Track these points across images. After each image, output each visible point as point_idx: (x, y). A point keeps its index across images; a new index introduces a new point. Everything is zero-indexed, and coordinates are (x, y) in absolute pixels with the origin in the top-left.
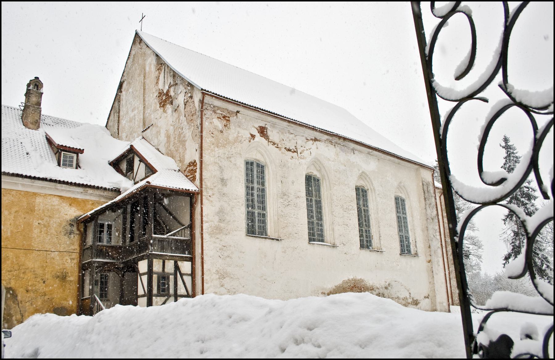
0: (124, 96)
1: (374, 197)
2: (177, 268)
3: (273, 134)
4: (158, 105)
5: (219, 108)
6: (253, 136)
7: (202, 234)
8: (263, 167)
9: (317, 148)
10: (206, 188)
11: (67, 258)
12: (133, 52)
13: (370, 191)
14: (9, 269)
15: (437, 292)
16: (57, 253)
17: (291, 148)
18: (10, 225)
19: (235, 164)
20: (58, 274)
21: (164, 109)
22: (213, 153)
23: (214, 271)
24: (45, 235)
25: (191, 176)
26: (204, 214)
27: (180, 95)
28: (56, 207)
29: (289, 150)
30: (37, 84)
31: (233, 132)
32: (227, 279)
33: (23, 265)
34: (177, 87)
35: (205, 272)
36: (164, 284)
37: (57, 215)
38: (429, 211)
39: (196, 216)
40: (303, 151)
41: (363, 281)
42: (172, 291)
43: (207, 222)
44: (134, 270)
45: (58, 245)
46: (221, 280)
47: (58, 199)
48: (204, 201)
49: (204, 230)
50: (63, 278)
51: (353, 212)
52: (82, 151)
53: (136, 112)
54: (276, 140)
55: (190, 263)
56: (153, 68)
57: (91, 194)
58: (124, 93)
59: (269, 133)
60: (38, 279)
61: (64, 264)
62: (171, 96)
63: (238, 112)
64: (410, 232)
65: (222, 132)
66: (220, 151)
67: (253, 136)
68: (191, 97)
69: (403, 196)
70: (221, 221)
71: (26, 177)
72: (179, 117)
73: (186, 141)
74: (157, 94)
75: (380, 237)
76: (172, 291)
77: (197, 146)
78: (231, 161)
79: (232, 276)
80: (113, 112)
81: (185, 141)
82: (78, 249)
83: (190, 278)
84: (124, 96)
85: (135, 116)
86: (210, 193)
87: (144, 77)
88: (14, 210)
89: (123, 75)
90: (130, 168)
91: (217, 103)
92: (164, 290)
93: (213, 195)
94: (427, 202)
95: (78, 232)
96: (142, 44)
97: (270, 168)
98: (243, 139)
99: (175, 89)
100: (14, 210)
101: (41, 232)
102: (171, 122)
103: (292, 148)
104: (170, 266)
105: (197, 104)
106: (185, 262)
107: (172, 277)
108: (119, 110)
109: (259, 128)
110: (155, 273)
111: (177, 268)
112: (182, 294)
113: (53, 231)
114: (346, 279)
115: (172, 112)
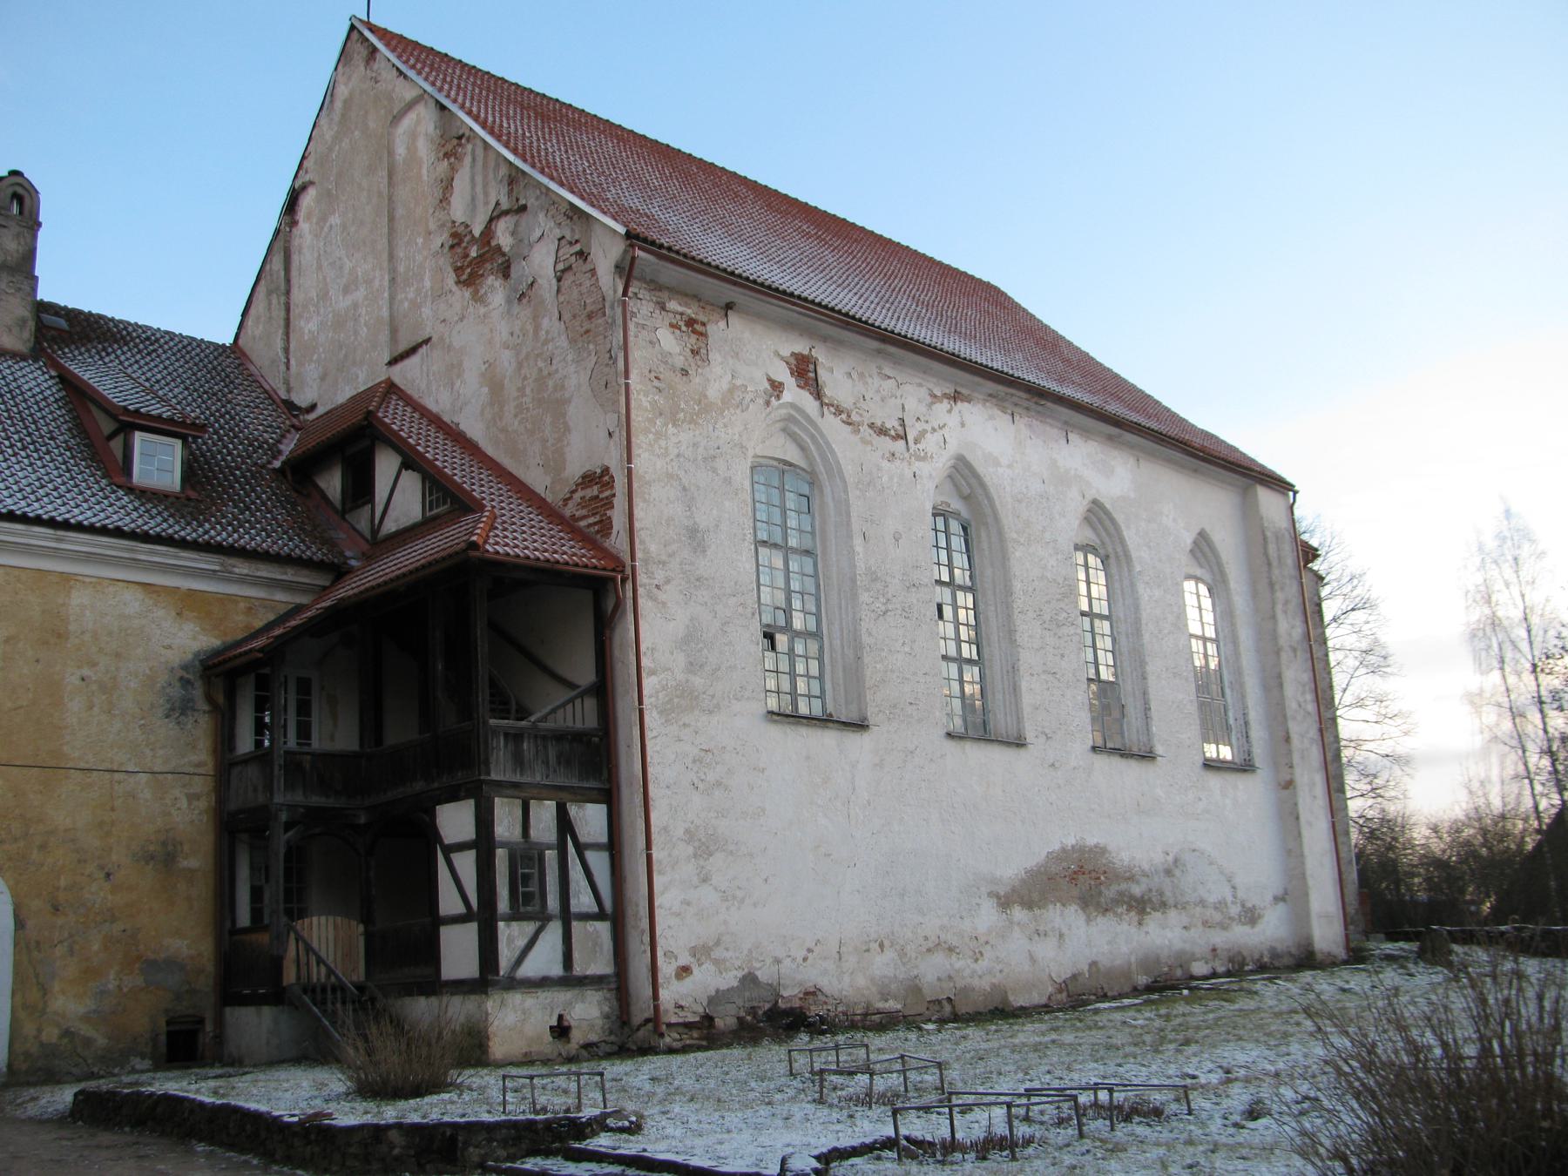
1: (1126, 582)
2: (565, 825)
4: (451, 278)
6: (777, 387)
9: (963, 425)
10: (646, 561)
15: (1310, 882)
16: (143, 777)
17: (888, 425)
19: (728, 481)
20: (152, 848)
21: (477, 292)
22: (663, 443)
23: (680, 832)
25: (592, 520)
26: (643, 648)
27: (537, 247)
29: (882, 431)
30: (20, 191)
31: (716, 378)
32: (718, 859)
34: (525, 219)
35: (654, 836)
36: (526, 879)
37: (139, 651)
39: (617, 653)
40: (923, 433)
42: (553, 903)
43: (653, 673)
44: (428, 836)
45: (148, 751)
46: (702, 862)
47: (139, 593)
49: (646, 700)
50: (164, 856)
53: (360, 295)
56: (424, 150)
57: (242, 580)
58: (304, 226)
59: (823, 375)
61: (169, 814)
62: (499, 248)
65: (685, 372)
67: (777, 387)
68: (582, 255)
70: (692, 667)
71: (37, 521)
73: (569, 401)
74: (442, 238)
76: (553, 903)
79: (732, 847)
80: (262, 288)
85: (355, 306)
86: (660, 575)
87: (390, 176)
92: (528, 898)
93: (668, 581)
95: (206, 708)
97: (827, 490)
98: (748, 398)
99: (516, 225)
101: (91, 708)
102: (505, 335)
104: (544, 816)
106: (589, 805)
107: (551, 856)
108: (288, 281)
110: (503, 845)
111: (565, 825)
112: (584, 909)
114: (1057, 847)
115: (509, 301)
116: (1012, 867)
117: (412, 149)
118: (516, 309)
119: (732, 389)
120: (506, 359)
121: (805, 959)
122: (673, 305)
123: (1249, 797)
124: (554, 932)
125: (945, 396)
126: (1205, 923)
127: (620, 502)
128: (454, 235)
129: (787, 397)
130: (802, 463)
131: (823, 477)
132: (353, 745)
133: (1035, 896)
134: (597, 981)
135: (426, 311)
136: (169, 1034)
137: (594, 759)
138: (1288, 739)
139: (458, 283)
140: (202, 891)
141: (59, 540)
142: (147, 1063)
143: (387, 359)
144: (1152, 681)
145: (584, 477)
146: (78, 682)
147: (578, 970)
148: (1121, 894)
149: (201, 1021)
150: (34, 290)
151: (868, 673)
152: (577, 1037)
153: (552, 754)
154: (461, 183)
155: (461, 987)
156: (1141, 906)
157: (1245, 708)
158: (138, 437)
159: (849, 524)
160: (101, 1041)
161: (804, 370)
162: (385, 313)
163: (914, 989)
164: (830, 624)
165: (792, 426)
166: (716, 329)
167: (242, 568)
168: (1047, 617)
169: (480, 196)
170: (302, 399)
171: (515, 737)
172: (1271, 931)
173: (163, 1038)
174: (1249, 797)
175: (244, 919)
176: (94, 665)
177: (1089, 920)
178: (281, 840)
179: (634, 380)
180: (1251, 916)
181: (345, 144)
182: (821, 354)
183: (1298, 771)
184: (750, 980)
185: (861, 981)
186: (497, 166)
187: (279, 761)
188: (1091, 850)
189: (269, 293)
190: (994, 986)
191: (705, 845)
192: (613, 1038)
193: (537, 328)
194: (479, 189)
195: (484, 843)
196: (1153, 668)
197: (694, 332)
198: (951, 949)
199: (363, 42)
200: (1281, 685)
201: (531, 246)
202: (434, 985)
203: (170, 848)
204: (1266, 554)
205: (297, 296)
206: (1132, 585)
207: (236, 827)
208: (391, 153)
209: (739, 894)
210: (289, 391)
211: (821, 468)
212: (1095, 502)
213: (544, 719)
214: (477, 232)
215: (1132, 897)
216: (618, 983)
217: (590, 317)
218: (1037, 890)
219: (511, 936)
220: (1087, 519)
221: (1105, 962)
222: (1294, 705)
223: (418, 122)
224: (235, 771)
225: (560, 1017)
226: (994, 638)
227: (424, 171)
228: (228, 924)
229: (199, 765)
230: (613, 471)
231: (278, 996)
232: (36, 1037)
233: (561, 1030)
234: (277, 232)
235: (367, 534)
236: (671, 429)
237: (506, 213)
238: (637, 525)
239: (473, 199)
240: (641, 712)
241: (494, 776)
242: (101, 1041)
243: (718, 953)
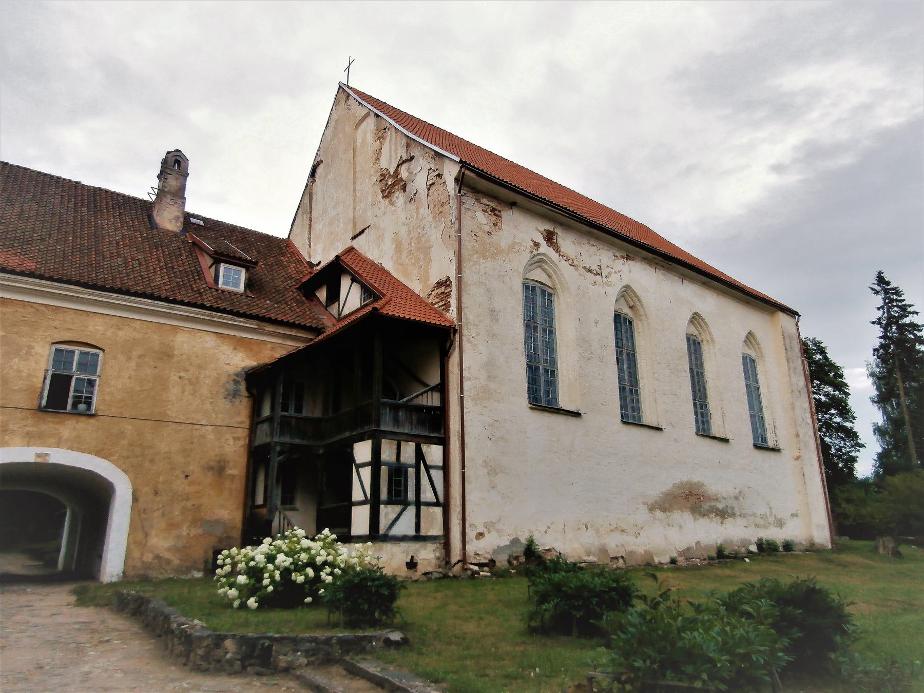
6: (537, 245)
7: (462, 399)
8: (550, 295)
10: (467, 324)
11: (228, 436)
12: (335, 117)
13: (705, 343)
14: (125, 454)
18: (130, 378)
20: (212, 463)
22: (477, 267)
23: (481, 462)
24: (190, 397)
25: (441, 304)
29: (590, 271)
30: (179, 159)
33: (150, 447)
38: (794, 379)
39: (450, 369)
42: (411, 496)
43: (469, 379)
44: (349, 459)
45: (213, 415)
47: (214, 337)
50: (219, 469)
51: (684, 374)
53: (340, 209)
54: (572, 255)
56: (370, 138)
57: (270, 334)
60: (177, 472)
64: (764, 410)
69: (753, 355)
70: (490, 378)
72: (417, 209)
74: (377, 177)
75: (724, 416)
76: (411, 496)
77: (452, 254)
80: (299, 215)
81: (430, 247)
85: (338, 214)
87: (355, 153)
88: (135, 354)
89: (317, 154)
93: (478, 334)
94: (791, 364)
98: (522, 248)
100: (135, 354)
101: (183, 392)
102: (404, 219)
104: (408, 452)
106: (433, 446)
107: (411, 472)
109: (545, 233)
110: (386, 464)
112: (428, 500)
113: (204, 391)
115: (405, 203)
117: (364, 139)
118: (409, 206)
120: (404, 231)
121: (546, 532)
122: (484, 201)
124: (411, 511)
125: (622, 257)
127: (454, 294)
128: (381, 175)
129: (541, 250)
133: (667, 505)
134: (433, 539)
135: (369, 213)
139: (383, 197)
140: (238, 486)
145: (438, 283)
146: (178, 379)
147: (423, 532)
148: (712, 507)
150: (184, 204)
152: (421, 569)
156: (723, 514)
160: (176, 562)
161: (550, 237)
162: (351, 216)
170: (315, 261)
175: (260, 500)
176: (187, 371)
177: (695, 520)
182: (559, 231)
188: (696, 484)
189: (303, 213)
190: (646, 551)
192: (440, 570)
194: (393, 152)
197: (495, 215)
198: (623, 531)
199: (344, 93)
203: (222, 464)
205: (314, 214)
207: (257, 456)
208: (355, 142)
215: (717, 509)
217: (442, 205)
219: (387, 513)
224: (259, 426)
225: (412, 557)
229: (241, 423)
232: (141, 558)
236: (482, 260)
237: (404, 162)
242: (176, 562)
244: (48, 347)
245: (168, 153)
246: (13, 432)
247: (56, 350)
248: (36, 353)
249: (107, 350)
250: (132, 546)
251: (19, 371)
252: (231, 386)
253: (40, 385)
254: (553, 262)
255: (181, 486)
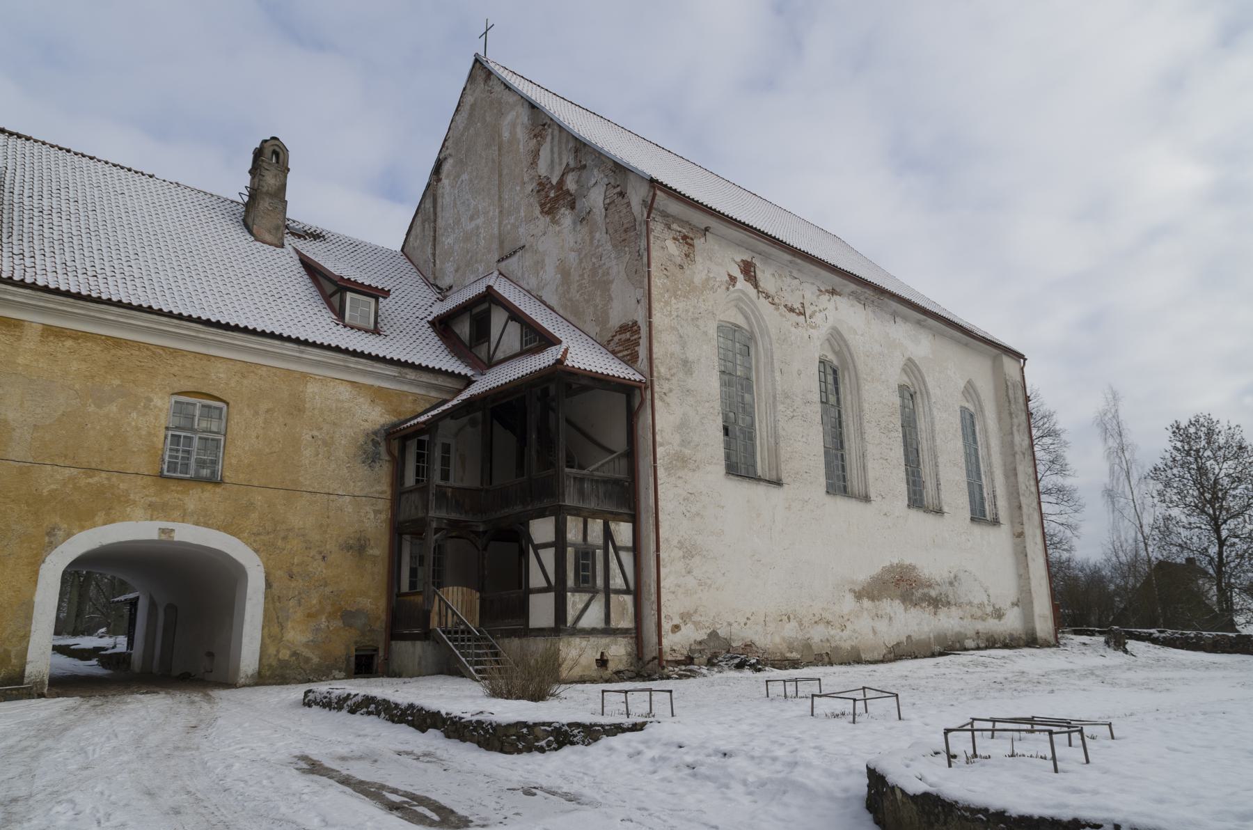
0: (448, 188)
1: (927, 409)
3: (766, 277)
4: (537, 210)
5: (676, 219)
6: (733, 279)
12: (470, 99)
14: (255, 530)
15: (1034, 595)
16: (348, 499)
19: (705, 333)
23: (675, 542)
28: (346, 405)
29: (792, 310)
31: (700, 270)
32: (697, 559)
34: (584, 174)
39: (640, 432)
41: (914, 568)
42: (600, 582)
43: (662, 445)
44: (517, 538)
48: (658, 403)
50: (358, 547)
51: (896, 434)
52: (386, 293)
53: (480, 221)
54: (772, 291)
55: (630, 525)
56: (521, 134)
57: (411, 383)
58: (445, 182)
60: (313, 553)
62: (568, 191)
63: (707, 229)
65: (681, 267)
66: (681, 305)
67: (733, 279)
70: (684, 443)
73: (612, 282)
76: (600, 582)
78: (698, 327)
80: (419, 219)
82: (389, 492)
83: (631, 554)
84: (448, 188)
85: (478, 227)
88: (264, 406)
90: (481, 329)
91: (674, 208)
93: (671, 391)
95: (387, 458)
96: (493, 82)
97: (760, 343)
102: (572, 244)
103: (797, 306)
104: (596, 527)
105: (637, 207)
107: (599, 553)
108: (435, 214)
110: (573, 545)
114: (888, 564)
115: (574, 223)
116: (864, 574)
117: (513, 133)
118: (579, 227)
119: (708, 279)
122: (675, 226)
123: (998, 541)
126: (972, 616)
127: (644, 342)
128: (540, 184)
130: (746, 326)
131: (758, 335)
132: (476, 484)
134: (624, 632)
135: (521, 230)
136: (357, 657)
137: (627, 495)
138: (1020, 507)
141: (302, 352)
142: (343, 674)
143: (497, 258)
144: (941, 467)
147: (613, 624)
148: (925, 595)
149: (376, 650)
151: (782, 452)
152: (612, 666)
153: (601, 490)
154: (545, 153)
155: (541, 632)
156: (936, 603)
157: (994, 487)
158: (349, 295)
159: (772, 363)
160: (315, 660)
161: (748, 270)
162: (496, 231)
163: (808, 646)
164: (760, 422)
165: (739, 304)
166: (699, 242)
167: (411, 375)
168: (883, 425)
169: (557, 160)
171: (581, 480)
172: (1012, 623)
173: (353, 659)
174: (998, 541)
175: (405, 587)
177: (906, 610)
178: (432, 538)
179: (653, 268)
180: (999, 614)
181: (472, 131)
183: (1026, 527)
184: (713, 635)
185: (777, 640)
186: (568, 141)
187: (432, 491)
189: (423, 222)
190: (853, 647)
191: (689, 552)
193: (592, 239)
194: (556, 155)
195: (560, 543)
196: (942, 460)
198: (828, 623)
200: (1016, 475)
201: (589, 189)
202: (527, 632)
204: (1007, 395)
206: (930, 409)
209: (709, 582)
210: (435, 278)
211: (756, 330)
212: (909, 359)
213: (597, 469)
214: (554, 182)
215: (930, 597)
216: (637, 634)
217: (626, 231)
218: (874, 591)
219: (575, 601)
220: (904, 370)
221: (915, 636)
222: (1024, 487)
223: (517, 117)
224: (404, 497)
225: (602, 654)
226: (852, 436)
227: (521, 146)
228: (396, 590)
229: (381, 493)
230: (640, 323)
231: (427, 635)
233: (602, 662)
234: (429, 185)
235: (485, 359)
236: (674, 301)
238: (654, 356)
239: (552, 161)
240: (655, 468)
241: (567, 503)
243: (696, 618)
244: (167, 399)
245: (265, 141)
246: (134, 502)
247: (203, 406)
248: (156, 407)
249: (231, 403)
250: (268, 641)
251: (138, 429)
252: (370, 448)
253: (161, 446)
254: (751, 301)
255: (318, 568)
